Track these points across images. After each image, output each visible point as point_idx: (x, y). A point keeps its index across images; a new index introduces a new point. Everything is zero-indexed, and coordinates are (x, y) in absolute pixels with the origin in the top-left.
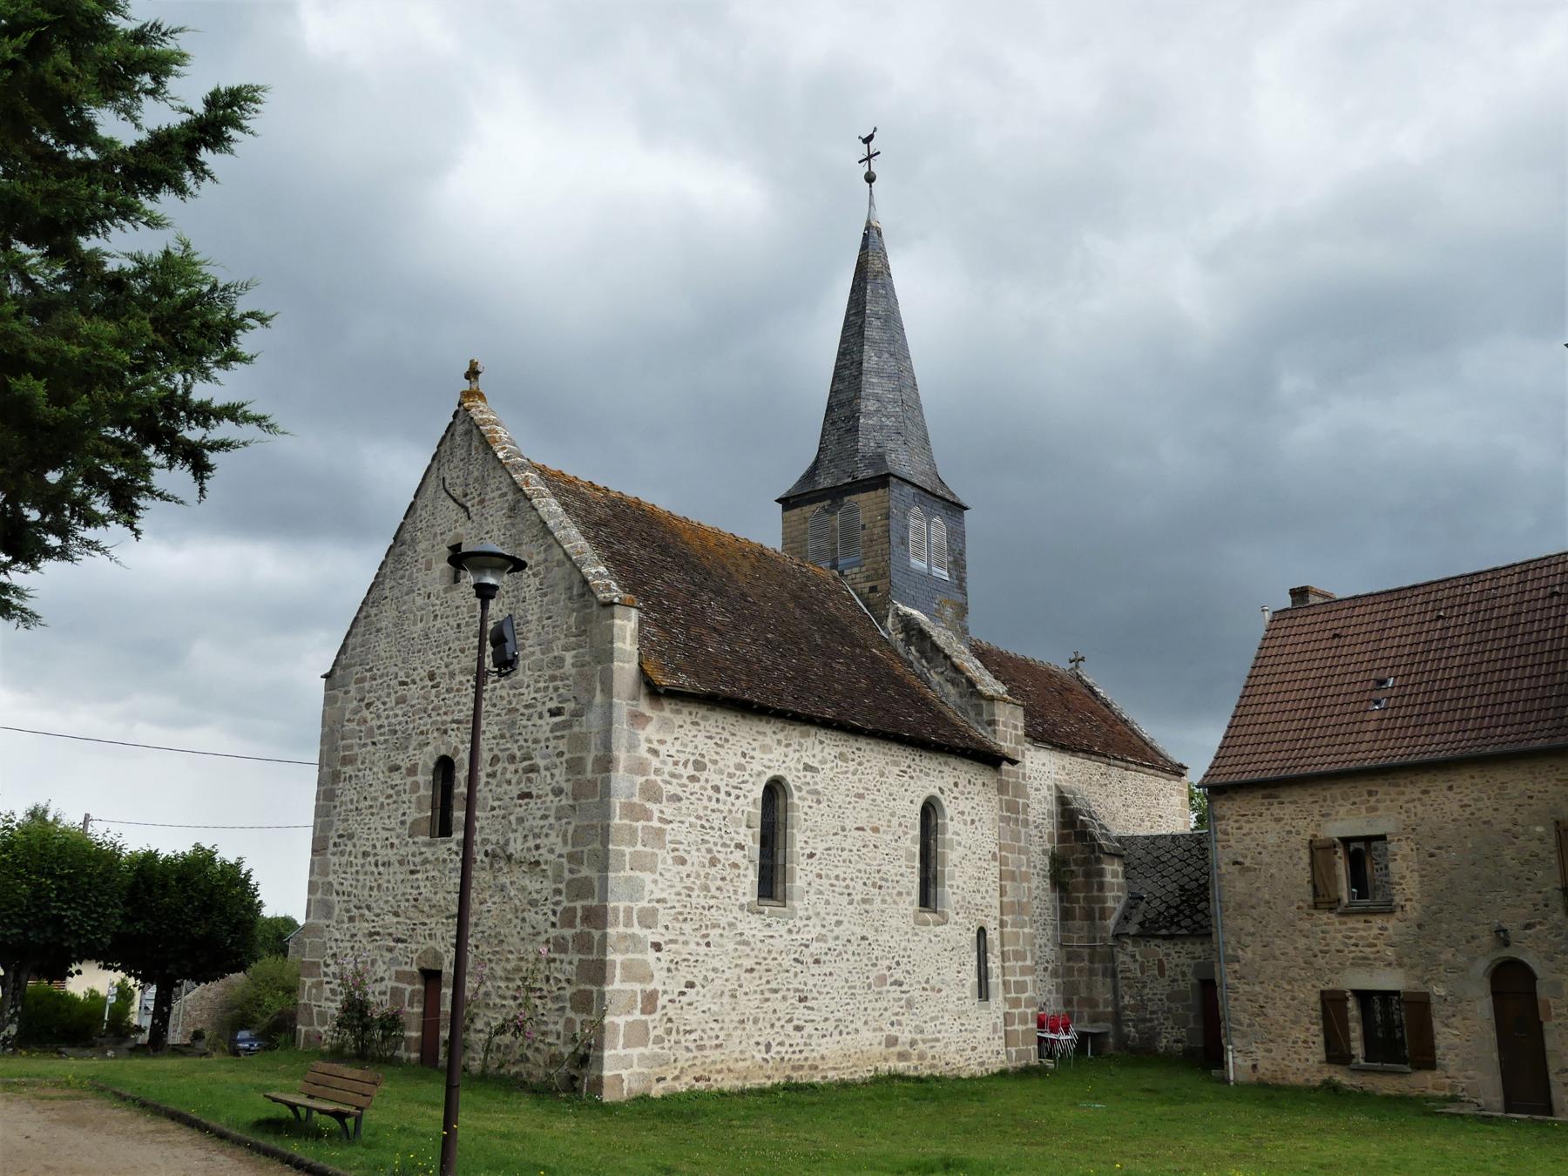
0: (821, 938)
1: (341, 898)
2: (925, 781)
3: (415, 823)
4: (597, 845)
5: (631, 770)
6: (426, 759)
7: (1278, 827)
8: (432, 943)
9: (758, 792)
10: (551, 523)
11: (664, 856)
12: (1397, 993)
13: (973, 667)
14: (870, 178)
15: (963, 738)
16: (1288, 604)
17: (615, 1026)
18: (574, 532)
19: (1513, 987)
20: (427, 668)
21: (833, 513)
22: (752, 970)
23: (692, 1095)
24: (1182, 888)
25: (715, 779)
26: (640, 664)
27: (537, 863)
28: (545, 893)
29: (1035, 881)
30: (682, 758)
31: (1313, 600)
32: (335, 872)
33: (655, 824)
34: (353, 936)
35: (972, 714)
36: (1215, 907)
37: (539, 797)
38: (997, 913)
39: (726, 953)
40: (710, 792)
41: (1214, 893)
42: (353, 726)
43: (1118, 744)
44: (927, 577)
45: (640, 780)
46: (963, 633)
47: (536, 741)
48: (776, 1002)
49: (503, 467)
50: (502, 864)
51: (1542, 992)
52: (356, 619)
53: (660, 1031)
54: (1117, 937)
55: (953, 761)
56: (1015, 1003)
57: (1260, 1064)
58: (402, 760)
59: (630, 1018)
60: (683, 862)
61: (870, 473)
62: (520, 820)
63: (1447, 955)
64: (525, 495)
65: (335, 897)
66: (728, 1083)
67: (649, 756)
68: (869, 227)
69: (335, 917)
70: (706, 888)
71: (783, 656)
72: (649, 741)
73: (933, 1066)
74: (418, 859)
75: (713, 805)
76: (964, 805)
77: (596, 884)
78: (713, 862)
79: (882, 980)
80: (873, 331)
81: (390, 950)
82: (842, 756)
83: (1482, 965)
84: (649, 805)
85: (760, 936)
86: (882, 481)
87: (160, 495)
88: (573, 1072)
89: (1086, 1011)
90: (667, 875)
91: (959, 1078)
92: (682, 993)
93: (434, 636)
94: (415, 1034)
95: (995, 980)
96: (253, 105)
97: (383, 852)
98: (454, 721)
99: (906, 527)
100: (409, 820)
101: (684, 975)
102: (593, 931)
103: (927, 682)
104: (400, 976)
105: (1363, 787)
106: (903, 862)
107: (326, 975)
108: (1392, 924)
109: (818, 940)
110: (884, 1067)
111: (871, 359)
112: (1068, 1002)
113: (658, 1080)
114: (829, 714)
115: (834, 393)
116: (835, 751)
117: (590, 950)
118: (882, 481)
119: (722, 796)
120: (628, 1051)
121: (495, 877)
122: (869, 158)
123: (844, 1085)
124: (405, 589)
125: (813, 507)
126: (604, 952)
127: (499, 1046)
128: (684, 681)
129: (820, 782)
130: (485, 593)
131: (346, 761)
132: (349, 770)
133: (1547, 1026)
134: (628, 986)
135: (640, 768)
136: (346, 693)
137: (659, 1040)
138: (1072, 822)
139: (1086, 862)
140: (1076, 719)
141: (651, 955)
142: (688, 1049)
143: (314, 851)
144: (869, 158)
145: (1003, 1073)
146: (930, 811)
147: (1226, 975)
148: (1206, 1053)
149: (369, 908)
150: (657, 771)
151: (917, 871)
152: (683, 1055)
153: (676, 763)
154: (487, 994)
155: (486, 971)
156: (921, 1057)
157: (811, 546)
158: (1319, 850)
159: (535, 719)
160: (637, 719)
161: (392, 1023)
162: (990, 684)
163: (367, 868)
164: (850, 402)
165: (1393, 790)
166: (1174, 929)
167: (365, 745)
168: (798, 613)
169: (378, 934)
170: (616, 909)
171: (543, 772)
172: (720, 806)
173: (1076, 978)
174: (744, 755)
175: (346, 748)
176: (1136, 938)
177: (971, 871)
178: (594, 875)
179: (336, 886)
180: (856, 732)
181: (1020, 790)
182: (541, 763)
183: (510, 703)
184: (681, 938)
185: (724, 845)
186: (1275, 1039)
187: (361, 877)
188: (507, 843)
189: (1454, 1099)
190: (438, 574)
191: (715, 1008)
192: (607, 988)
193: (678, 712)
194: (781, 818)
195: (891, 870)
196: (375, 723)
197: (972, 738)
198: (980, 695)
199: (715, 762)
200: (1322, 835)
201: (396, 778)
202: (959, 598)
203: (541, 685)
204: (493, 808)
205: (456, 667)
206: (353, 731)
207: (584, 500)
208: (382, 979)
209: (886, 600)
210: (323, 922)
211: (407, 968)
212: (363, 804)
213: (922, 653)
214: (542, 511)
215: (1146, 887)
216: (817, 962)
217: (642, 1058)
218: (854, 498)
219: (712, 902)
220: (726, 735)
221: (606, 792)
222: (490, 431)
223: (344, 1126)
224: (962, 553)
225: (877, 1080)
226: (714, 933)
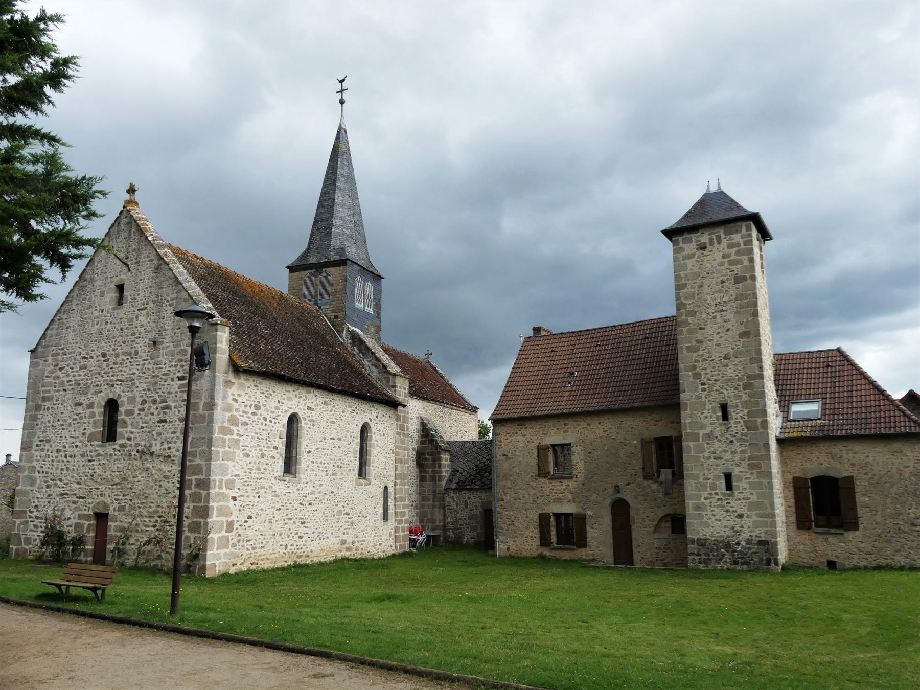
0: (312, 493)
1: (41, 475)
2: (363, 415)
3: (92, 434)
4: (205, 448)
5: (224, 410)
6: (100, 400)
7: (524, 439)
8: (103, 499)
9: (285, 421)
10: (181, 278)
11: (239, 453)
12: (572, 514)
13: (385, 358)
14: (342, 102)
15: (381, 394)
16: (532, 334)
17: (213, 539)
18: (194, 284)
19: (620, 511)
20: (101, 350)
21: (317, 276)
22: (279, 509)
23: (250, 572)
24: (477, 466)
25: (265, 414)
26: (230, 356)
27: (169, 457)
28: (173, 472)
29: (410, 462)
30: (249, 403)
31: (543, 333)
32: (37, 461)
33: (235, 437)
34: (49, 495)
35: (384, 382)
36: (494, 476)
37: (171, 422)
38: (393, 479)
39: (268, 501)
40: (262, 421)
41: (494, 469)
42: (51, 380)
43: (448, 397)
44: (363, 312)
45: (228, 414)
46: (378, 340)
47: (169, 393)
48: (290, 524)
49: (152, 245)
50: (147, 457)
51: (632, 513)
52: (53, 320)
53: (235, 541)
54: (446, 489)
55: (377, 406)
56: (400, 522)
57: (511, 547)
58: (82, 399)
59: (220, 535)
60: (248, 456)
61: (337, 257)
62: (159, 434)
63: (594, 497)
64: (165, 262)
65: (37, 474)
66: (266, 565)
67: (233, 403)
68: (340, 128)
69: (37, 485)
70: (259, 469)
71: (296, 351)
72: (233, 395)
73: (362, 553)
74: (94, 454)
75: (263, 427)
76: (380, 427)
77: (204, 468)
78: (263, 456)
79: (340, 512)
80: (341, 183)
81: (75, 503)
82: (325, 403)
83: (608, 501)
84: (232, 427)
85: (284, 492)
86: (343, 262)
87: (46, 280)
88: (189, 563)
89: (430, 525)
90: (240, 463)
91: (373, 559)
92: (246, 522)
93: (105, 333)
94: (90, 547)
95: (391, 511)
96: (75, 67)
97: (71, 449)
98: (118, 380)
99: (354, 286)
100: (88, 433)
101: (247, 512)
102: (202, 492)
103: (363, 365)
104: (80, 517)
105: (562, 422)
106: (352, 455)
107: (30, 517)
108: (572, 484)
109: (311, 493)
110: (340, 555)
111: (339, 198)
112: (421, 521)
113: (233, 565)
114: (321, 382)
115: (318, 213)
116: (322, 400)
117: (200, 501)
118: (343, 262)
119: (268, 423)
120: (219, 551)
121: (143, 464)
122: (342, 91)
123: (321, 564)
124: (86, 306)
125: (306, 272)
126: (208, 502)
127: (144, 552)
128: (252, 365)
129: (314, 415)
130: (193, 330)
131: (44, 399)
132: (47, 404)
133: (633, 527)
134: (219, 519)
135: (228, 408)
136: (45, 361)
137: (234, 545)
138: (427, 434)
139: (433, 454)
140: (434, 388)
141: (232, 503)
142: (248, 549)
143: (22, 449)
144: (342, 91)
145: (393, 556)
146: (365, 429)
147: (497, 507)
148: (486, 543)
149: (60, 480)
150: (237, 410)
151: (358, 459)
152: (245, 552)
153: (246, 406)
154: (137, 525)
155: (137, 513)
156: (357, 549)
157: (304, 292)
158: (542, 450)
159: (169, 381)
160: (228, 383)
161: (78, 542)
162: (394, 368)
163: (60, 458)
164: (327, 219)
165: (575, 423)
166: (473, 486)
167: (59, 391)
168: (301, 328)
169: (67, 494)
170: (214, 480)
171: (173, 410)
172: (267, 428)
173: (426, 509)
174: (279, 402)
175: (44, 392)
176: (454, 490)
177: (383, 459)
178: (203, 463)
179: (38, 468)
180: (332, 391)
181: (406, 420)
182: (173, 405)
183: (154, 372)
184: (246, 494)
185: (268, 447)
186: (518, 535)
187: (55, 463)
188: (151, 446)
189: (593, 560)
190: (108, 299)
191: (261, 529)
192: (209, 520)
193: (248, 380)
194: (295, 434)
195: (346, 459)
196: (65, 379)
197: (385, 394)
198: (389, 373)
199: (265, 405)
200: (543, 443)
201: (80, 410)
202: (377, 323)
203: (173, 364)
204: (142, 428)
205: (120, 351)
206: (50, 383)
207: (192, 264)
208: (69, 519)
209: (343, 323)
210: (28, 488)
211: (86, 512)
212: (56, 423)
213: (360, 351)
214: (175, 271)
215: (460, 466)
216: (310, 504)
217: (226, 554)
218: (328, 269)
219: (261, 476)
220: (270, 392)
221: (211, 421)
222: (143, 224)
223: (96, 595)
224: (379, 301)
225: (336, 561)
226: (262, 491)
